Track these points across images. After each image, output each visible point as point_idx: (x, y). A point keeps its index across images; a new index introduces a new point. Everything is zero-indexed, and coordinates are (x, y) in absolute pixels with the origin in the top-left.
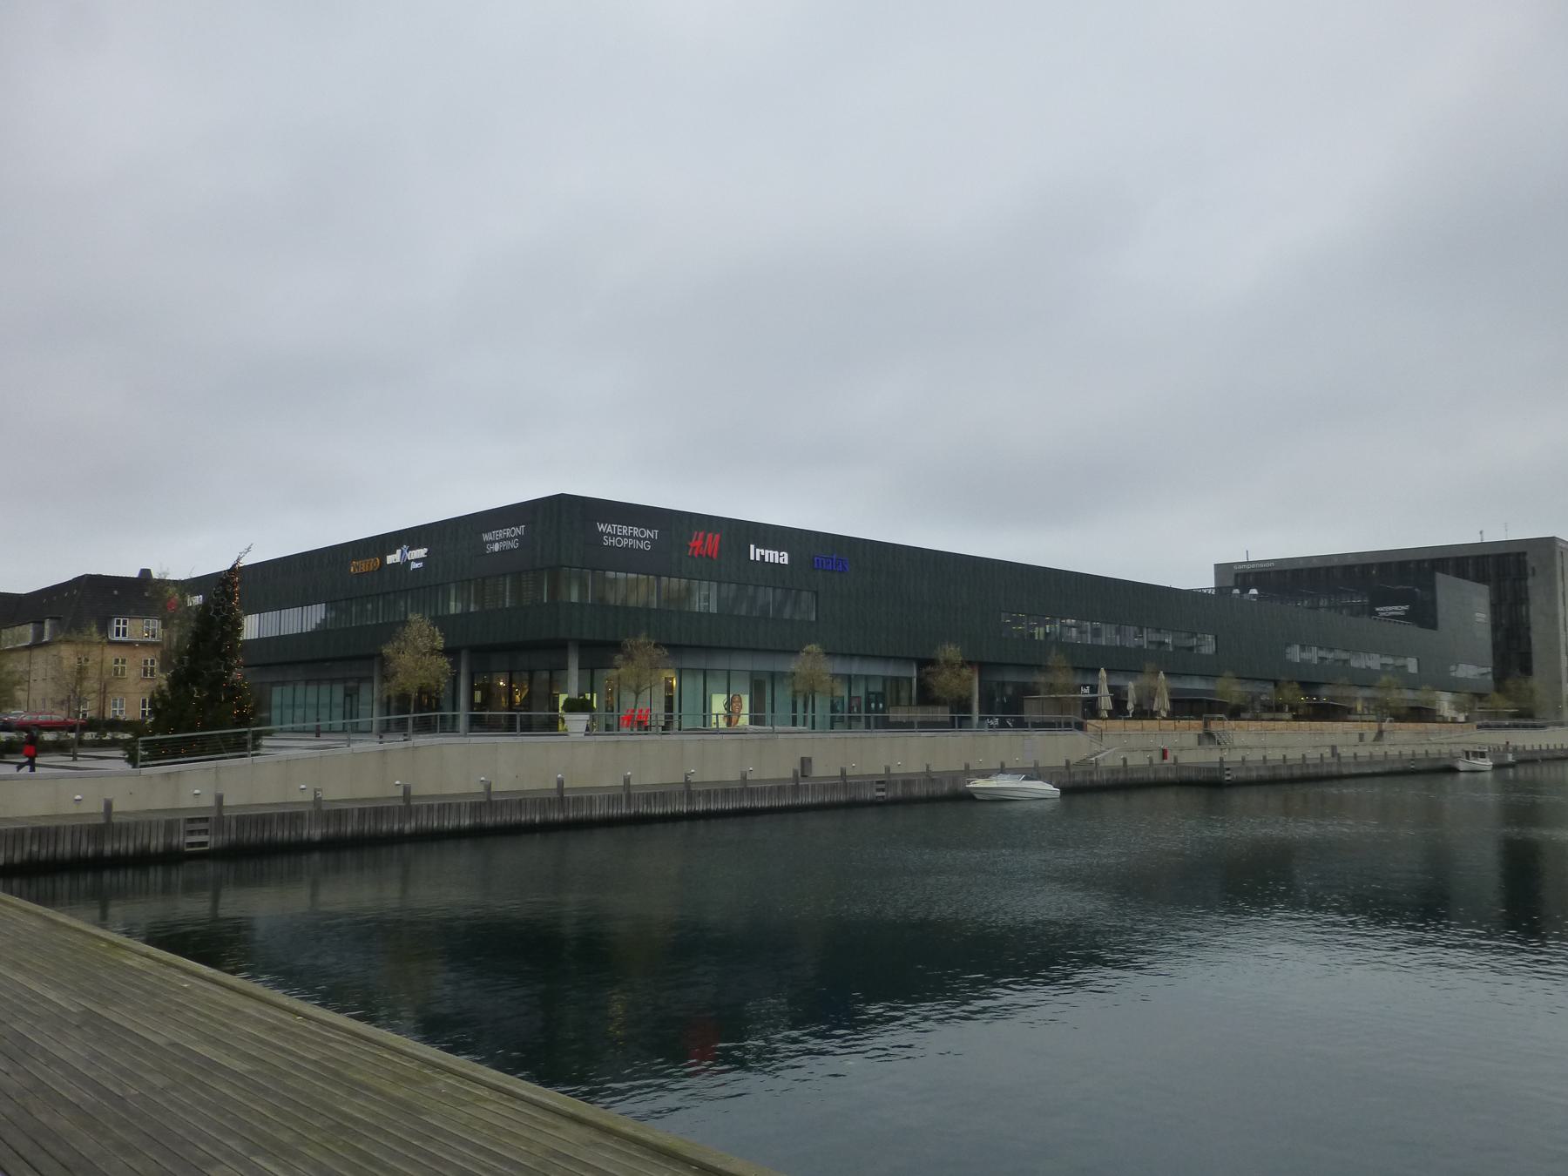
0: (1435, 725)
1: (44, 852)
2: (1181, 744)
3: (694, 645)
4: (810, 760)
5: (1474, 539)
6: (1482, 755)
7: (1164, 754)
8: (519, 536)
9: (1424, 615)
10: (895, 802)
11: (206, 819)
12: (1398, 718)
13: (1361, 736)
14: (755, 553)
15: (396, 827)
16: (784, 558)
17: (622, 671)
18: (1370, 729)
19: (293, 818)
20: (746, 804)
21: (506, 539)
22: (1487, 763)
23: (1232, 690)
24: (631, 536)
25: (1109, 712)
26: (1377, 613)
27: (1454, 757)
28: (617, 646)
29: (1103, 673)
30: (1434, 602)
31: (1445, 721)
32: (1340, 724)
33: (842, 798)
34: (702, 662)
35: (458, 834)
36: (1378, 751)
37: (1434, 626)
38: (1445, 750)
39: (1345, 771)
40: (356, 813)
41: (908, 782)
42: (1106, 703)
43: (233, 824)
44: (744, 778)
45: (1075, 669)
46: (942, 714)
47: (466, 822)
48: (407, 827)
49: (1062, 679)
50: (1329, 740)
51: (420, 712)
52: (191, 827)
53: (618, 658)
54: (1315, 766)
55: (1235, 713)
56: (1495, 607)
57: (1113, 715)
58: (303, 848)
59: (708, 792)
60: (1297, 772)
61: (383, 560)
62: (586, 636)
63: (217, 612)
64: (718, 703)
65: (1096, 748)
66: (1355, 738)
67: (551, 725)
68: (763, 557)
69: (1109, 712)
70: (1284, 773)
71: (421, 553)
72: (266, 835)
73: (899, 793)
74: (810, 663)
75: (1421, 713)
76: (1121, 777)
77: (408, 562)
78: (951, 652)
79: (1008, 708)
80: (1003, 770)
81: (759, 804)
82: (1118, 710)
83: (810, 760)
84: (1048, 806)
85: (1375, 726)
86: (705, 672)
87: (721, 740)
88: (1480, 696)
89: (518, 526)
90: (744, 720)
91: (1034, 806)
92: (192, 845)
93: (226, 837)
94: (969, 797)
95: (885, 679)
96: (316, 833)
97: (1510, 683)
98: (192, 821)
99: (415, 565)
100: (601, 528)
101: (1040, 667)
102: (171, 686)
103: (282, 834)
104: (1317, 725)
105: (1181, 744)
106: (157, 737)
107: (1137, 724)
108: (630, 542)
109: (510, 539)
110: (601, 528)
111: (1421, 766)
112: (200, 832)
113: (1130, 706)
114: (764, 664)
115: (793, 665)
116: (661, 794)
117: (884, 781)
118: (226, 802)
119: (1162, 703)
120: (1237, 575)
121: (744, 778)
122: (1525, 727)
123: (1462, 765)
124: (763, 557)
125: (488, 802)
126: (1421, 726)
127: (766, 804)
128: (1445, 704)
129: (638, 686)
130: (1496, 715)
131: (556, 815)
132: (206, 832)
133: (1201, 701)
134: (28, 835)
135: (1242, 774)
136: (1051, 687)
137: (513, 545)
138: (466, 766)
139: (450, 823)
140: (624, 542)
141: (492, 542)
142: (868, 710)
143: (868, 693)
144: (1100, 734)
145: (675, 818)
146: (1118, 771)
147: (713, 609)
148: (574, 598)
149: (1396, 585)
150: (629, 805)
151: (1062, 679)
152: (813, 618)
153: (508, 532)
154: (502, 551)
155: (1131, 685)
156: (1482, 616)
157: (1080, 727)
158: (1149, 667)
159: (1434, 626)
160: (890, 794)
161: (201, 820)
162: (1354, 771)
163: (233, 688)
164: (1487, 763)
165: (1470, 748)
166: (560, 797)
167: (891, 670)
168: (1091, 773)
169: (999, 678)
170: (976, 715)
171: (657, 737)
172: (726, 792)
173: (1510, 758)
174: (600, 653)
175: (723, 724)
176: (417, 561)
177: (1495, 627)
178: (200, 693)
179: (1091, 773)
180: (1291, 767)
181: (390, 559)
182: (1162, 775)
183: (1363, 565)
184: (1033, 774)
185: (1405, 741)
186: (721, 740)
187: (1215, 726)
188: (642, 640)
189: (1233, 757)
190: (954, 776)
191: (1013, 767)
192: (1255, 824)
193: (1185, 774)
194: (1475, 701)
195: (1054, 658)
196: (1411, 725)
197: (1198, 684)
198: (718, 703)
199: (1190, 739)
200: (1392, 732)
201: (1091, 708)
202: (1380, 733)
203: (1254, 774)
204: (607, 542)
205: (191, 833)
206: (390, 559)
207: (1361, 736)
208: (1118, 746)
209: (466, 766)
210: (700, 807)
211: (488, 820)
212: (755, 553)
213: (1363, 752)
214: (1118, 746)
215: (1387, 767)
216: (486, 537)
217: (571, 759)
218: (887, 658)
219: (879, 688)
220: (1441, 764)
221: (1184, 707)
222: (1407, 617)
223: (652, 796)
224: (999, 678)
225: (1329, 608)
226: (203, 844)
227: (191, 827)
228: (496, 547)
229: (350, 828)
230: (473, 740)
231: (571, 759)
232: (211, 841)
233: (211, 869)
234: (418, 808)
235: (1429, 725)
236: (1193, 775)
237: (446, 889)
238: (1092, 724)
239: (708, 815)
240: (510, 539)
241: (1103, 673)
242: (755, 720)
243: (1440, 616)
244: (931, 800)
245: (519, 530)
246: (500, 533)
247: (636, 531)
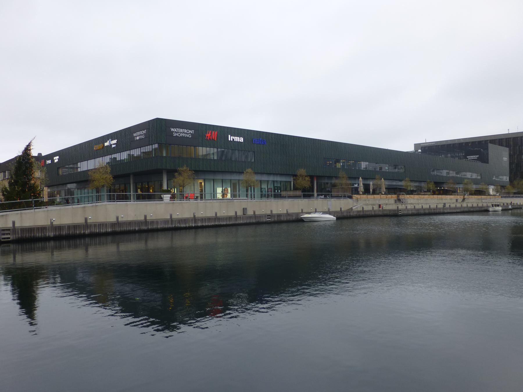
0: (485, 197)
1: (27, 235)
2: (388, 202)
3: (206, 170)
4: (246, 209)
5: (506, 132)
6: (498, 206)
7: (380, 206)
8: (144, 134)
9: (484, 159)
10: (275, 222)
11: (9, 230)
12: (471, 194)
13: (457, 200)
14: (231, 138)
15: (82, 232)
16: (242, 140)
17: (179, 179)
18: (460, 198)
19: (43, 229)
20: (217, 223)
21: (140, 135)
22: (500, 208)
23: (412, 185)
24: (184, 132)
25: (363, 192)
26: (467, 158)
27: (488, 206)
28: (176, 171)
29: (361, 179)
30: (488, 154)
31: (490, 195)
32: (449, 196)
33: (254, 221)
34: (211, 177)
35: (107, 234)
36: (465, 205)
37: (488, 163)
38: (485, 205)
39: (446, 211)
40: (67, 227)
41: (279, 215)
42: (361, 189)
43: (20, 231)
44: (52, 223)
45: (411, 181)
46: (299, 193)
47: (109, 230)
48: (87, 232)
49: (344, 181)
50: (444, 201)
51: (119, 194)
52: (3, 232)
53: (176, 174)
54: (434, 209)
55: (411, 192)
56: (511, 156)
57: (364, 193)
58: (48, 239)
59: (203, 219)
60: (427, 211)
61: (104, 145)
62: (318, 175)
63: (23, 160)
64: (219, 190)
65: (355, 204)
66: (455, 201)
67: (161, 199)
68: (233, 139)
69: (363, 192)
70: (422, 212)
71: (115, 141)
72: (32, 235)
73: (276, 219)
74: (249, 176)
75: (479, 192)
76: (361, 214)
77: (111, 145)
78: (302, 171)
79: (326, 192)
80: (316, 212)
81: (222, 223)
82: (367, 191)
83: (246, 209)
84: (332, 222)
85: (462, 197)
86: (213, 180)
87: (219, 201)
88: (503, 187)
89: (144, 130)
90: (229, 196)
91: (328, 223)
92: (4, 238)
93: (17, 236)
94: (302, 220)
95: (281, 182)
96: (52, 234)
97: (515, 183)
98: (4, 230)
99: (113, 146)
100: (172, 130)
101: (337, 177)
102: (10, 184)
103: (39, 235)
104: (440, 196)
105: (388, 202)
106: (18, 201)
107: (372, 196)
108: (184, 135)
109: (142, 135)
110: (172, 130)
111: (475, 210)
112: (7, 234)
113: (371, 190)
114: (235, 177)
115: (242, 177)
116: (185, 220)
117: (270, 216)
118: (148, 218)
119: (384, 190)
120: (422, 147)
121: (52, 223)
122: (519, 197)
123: (491, 209)
124: (233, 139)
125: (118, 223)
126: (479, 197)
127: (225, 223)
128: (491, 190)
129: (184, 184)
130: (509, 193)
131: (144, 228)
132: (9, 234)
133: (396, 188)
134: (97, 225)
135: (406, 212)
136: (342, 185)
137: (143, 137)
138: (131, 211)
139: (103, 230)
140: (181, 135)
141: (137, 136)
142: (275, 192)
143: (274, 187)
144: (357, 200)
145: (190, 228)
146: (360, 211)
147: (215, 158)
148: (164, 155)
149: (475, 149)
150: (172, 224)
151: (344, 181)
152: (253, 160)
153: (141, 133)
154: (140, 139)
155: (371, 183)
156: (506, 159)
157: (350, 197)
158: (377, 177)
159: (488, 163)
160: (273, 220)
161: (7, 230)
162: (449, 211)
163: (31, 187)
164: (500, 208)
165: (494, 203)
166: (146, 222)
167: (284, 179)
168: (350, 212)
169: (323, 181)
170: (315, 194)
171: (133, 203)
172: (209, 219)
173: (510, 207)
174: (172, 173)
175: (221, 198)
176: (114, 144)
177: (511, 164)
178: (18, 188)
179: (350, 212)
180: (425, 210)
181: (106, 144)
182: (377, 213)
183: (466, 143)
184: (329, 213)
185: (473, 201)
186: (219, 201)
187: (401, 197)
188: (185, 168)
189: (409, 207)
190: (298, 214)
191: (320, 211)
192: (411, 228)
193: (385, 213)
194: (502, 189)
195: (341, 174)
196: (476, 196)
197: (394, 183)
198: (219, 190)
199: (392, 201)
200: (468, 199)
201: (356, 191)
202: (464, 199)
203: (410, 212)
204: (175, 135)
205: (4, 234)
206: (106, 144)
207: (457, 200)
208: (363, 203)
209: (131, 211)
210: (200, 224)
211: (118, 229)
212: (231, 138)
213: (459, 205)
214: (363, 203)
215: (462, 210)
216: (135, 135)
217: (161, 209)
218: (281, 175)
219: (279, 185)
220: (483, 209)
221: (391, 190)
222: (478, 159)
223: (180, 221)
224: (323, 181)
225: (452, 157)
226: (9, 238)
227: (3, 232)
228: (138, 138)
229: (64, 232)
230: (138, 202)
231: (161, 209)
232: (11, 237)
233: (12, 246)
234: (91, 226)
235: (483, 196)
236: (388, 213)
237: (105, 253)
238: (355, 196)
239: (202, 227)
240: (142, 135)
241: (361, 179)
242: (233, 196)
243: (489, 158)
244: (288, 222)
245: (144, 132)
246: (138, 133)
247: (185, 131)
